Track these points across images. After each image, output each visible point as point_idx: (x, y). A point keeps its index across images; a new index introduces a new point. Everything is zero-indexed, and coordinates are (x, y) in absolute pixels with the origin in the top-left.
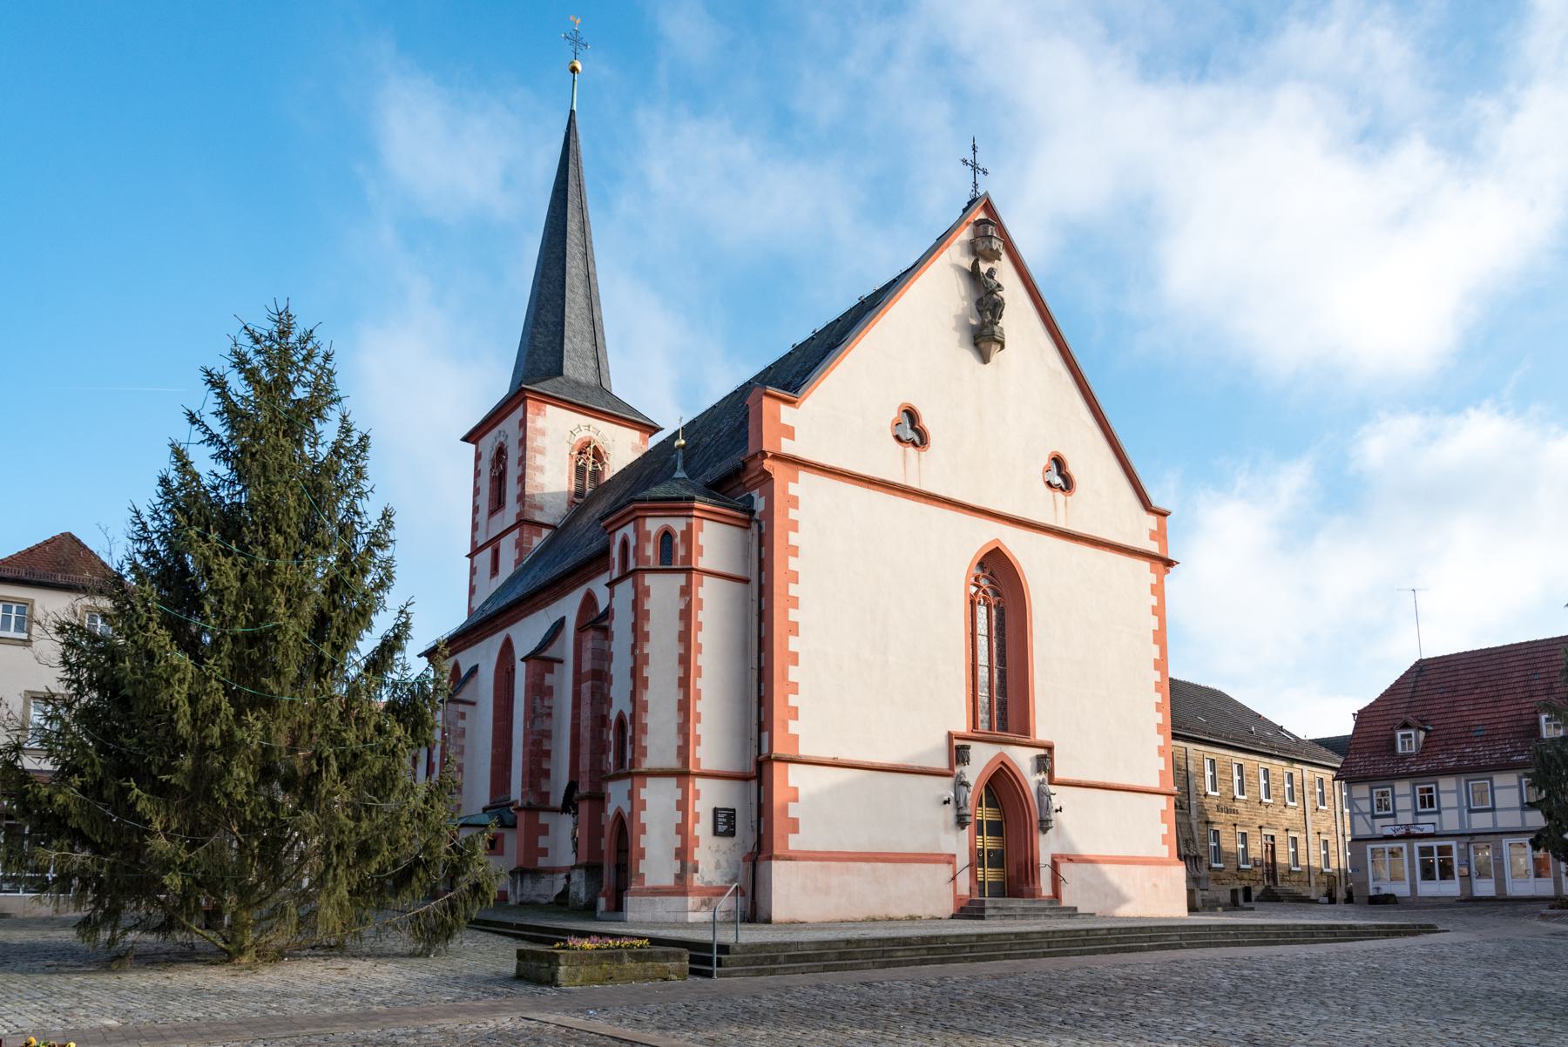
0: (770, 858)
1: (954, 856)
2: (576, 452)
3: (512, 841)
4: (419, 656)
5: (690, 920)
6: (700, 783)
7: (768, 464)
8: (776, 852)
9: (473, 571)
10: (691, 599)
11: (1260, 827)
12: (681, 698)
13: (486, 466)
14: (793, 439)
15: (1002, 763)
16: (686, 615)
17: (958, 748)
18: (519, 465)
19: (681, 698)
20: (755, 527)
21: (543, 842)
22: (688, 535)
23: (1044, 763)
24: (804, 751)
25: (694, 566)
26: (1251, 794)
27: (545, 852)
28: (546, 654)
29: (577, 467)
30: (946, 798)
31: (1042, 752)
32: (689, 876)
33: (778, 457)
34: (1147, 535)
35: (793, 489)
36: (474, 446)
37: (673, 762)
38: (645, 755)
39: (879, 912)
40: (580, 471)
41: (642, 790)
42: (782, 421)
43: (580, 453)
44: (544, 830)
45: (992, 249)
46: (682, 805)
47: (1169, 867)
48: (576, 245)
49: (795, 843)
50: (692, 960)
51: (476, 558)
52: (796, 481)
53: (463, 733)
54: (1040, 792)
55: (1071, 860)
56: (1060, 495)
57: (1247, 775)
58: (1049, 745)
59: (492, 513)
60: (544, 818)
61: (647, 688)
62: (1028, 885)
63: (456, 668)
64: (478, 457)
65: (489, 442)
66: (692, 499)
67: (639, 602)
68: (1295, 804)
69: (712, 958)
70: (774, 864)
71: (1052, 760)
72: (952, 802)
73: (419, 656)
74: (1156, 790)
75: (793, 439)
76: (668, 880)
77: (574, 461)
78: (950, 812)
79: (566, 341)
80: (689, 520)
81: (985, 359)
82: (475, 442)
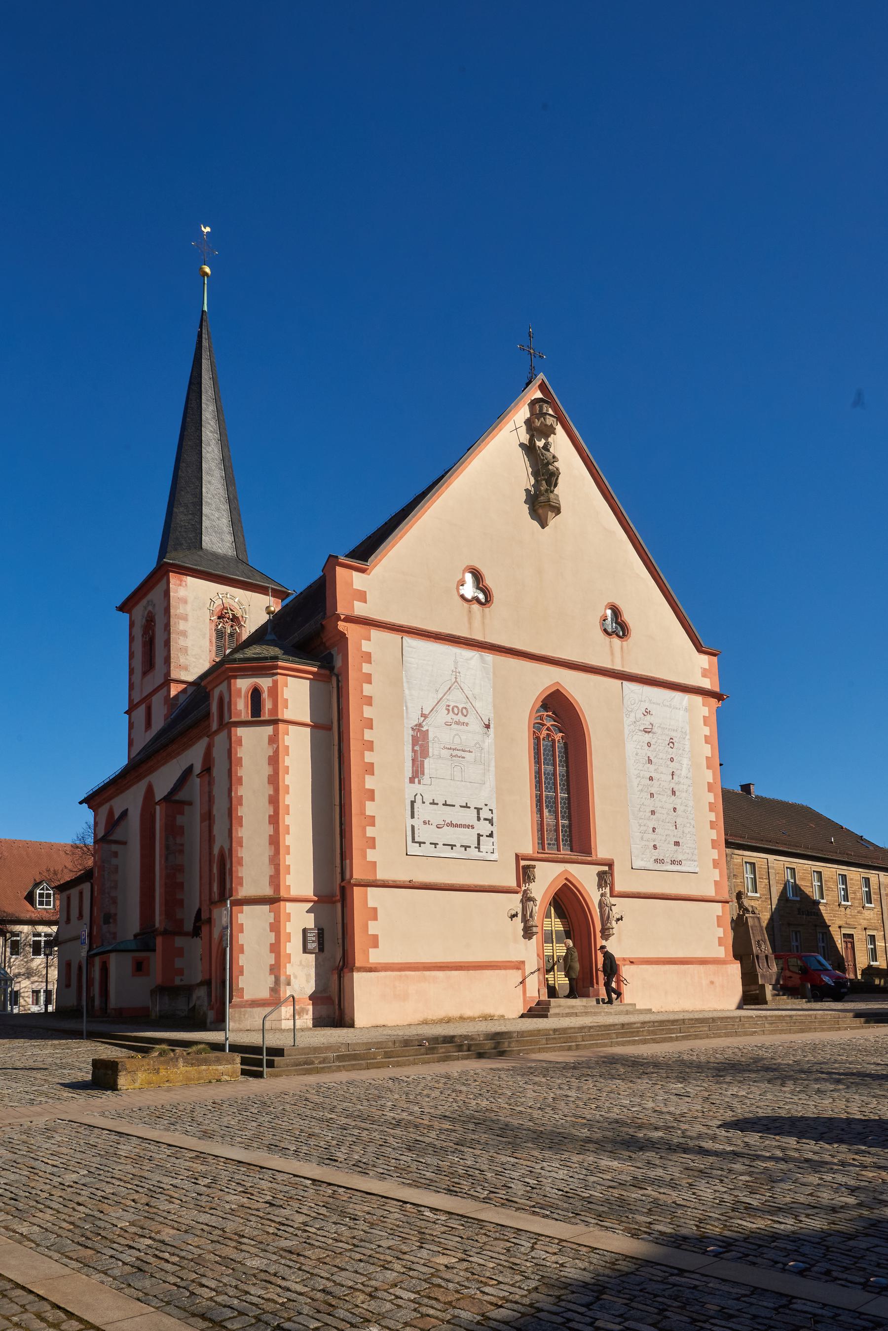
0: (352, 970)
1: (523, 962)
2: (216, 617)
3: (156, 960)
4: (81, 803)
5: (283, 1027)
6: (289, 907)
7: (341, 625)
8: (357, 964)
9: (131, 726)
10: (278, 747)
11: (840, 927)
12: (272, 833)
13: (138, 632)
14: (366, 602)
15: (566, 879)
16: (274, 761)
17: (526, 868)
18: (165, 630)
19: (272, 833)
20: (334, 679)
21: (178, 963)
22: (274, 691)
23: (605, 878)
24: (382, 875)
25: (280, 717)
26: (830, 898)
27: (181, 972)
28: (177, 797)
29: (217, 630)
30: (513, 912)
31: (606, 868)
32: (282, 989)
33: (350, 619)
34: (699, 672)
35: (366, 646)
36: (127, 615)
37: (267, 891)
38: (241, 884)
39: (454, 1013)
40: (220, 634)
41: (240, 915)
42: (355, 587)
43: (219, 618)
44: (180, 952)
45: (546, 425)
46: (276, 927)
47: (724, 966)
48: (211, 432)
49: (375, 956)
50: (244, 1062)
51: (134, 714)
52: (368, 639)
53: (116, 869)
54: (601, 905)
55: (632, 962)
56: (616, 641)
57: (826, 881)
58: (609, 862)
59: (145, 674)
60: (179, 941)
61: (242, 826)
62: (593, 987)
63: (111, 812)
64: (132, 625)
65: (139, 611)
66: (275, 658)
67: (233, 750)
68: (872, 905)
69: (262, 1060)
70: (357, 976)
71: (612, 875)
72: (520, 915)
73: (81, 803)
74: (712, 899)
75: (366, 602)
76: (265, 994)
77: (214, 624)
78: (518, 924)
79: (204, 518)
80: (275, 678)
81: (543, 525)
82: (129, 611)
